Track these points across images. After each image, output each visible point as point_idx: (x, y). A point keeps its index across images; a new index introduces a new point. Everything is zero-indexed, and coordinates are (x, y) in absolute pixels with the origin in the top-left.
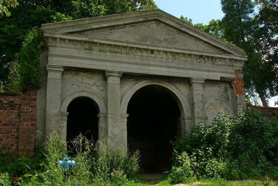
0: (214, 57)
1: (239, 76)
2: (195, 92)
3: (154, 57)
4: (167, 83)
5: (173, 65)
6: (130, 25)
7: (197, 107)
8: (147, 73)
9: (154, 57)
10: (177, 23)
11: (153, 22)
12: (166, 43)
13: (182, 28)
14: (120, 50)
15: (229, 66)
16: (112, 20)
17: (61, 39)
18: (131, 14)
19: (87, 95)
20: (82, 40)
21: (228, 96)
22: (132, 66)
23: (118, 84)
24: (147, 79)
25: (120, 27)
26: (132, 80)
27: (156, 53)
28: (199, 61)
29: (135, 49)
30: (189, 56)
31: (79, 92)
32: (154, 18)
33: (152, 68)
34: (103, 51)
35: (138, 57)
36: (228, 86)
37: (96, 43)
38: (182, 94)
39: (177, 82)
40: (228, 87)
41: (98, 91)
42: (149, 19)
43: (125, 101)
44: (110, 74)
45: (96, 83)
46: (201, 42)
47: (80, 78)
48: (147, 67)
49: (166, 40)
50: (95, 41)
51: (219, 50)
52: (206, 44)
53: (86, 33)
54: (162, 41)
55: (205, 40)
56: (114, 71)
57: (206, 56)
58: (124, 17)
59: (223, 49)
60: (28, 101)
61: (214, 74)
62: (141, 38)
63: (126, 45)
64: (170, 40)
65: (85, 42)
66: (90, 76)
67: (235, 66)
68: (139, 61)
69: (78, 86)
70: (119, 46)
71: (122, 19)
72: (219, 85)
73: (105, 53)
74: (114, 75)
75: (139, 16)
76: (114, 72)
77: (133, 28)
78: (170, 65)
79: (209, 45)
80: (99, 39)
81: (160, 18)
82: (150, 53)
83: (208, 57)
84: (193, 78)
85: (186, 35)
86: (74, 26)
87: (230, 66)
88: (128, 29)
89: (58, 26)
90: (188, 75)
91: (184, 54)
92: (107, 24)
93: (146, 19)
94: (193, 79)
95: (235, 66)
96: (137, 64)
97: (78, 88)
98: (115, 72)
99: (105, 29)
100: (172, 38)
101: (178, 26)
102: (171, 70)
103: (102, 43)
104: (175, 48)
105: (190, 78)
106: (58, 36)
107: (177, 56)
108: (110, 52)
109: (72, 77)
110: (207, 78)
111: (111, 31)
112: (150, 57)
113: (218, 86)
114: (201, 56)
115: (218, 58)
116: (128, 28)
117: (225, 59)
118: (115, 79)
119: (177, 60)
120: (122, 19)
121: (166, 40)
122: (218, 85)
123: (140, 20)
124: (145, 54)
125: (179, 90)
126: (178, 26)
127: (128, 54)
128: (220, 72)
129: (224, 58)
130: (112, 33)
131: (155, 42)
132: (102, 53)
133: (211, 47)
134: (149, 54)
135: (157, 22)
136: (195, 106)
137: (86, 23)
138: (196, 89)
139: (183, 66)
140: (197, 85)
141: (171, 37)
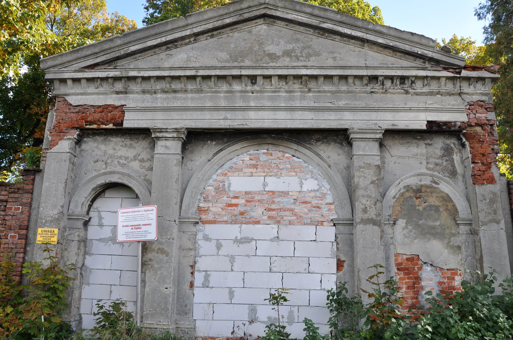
0: (407, 77)
1: (480, 117)
2: (357, 162)
3: (258, 92)
4: (293, 144)
5: (305, 104)
6: (207, 35)
7: (363, 196)
8: (241, 127)
9: (258, 92)
10: (312, 15)
11: (258, 21)
12: (288, 59)
13: (324, 22)
14: (182, 85)
15: (450, 94)
16: (167, 31)
17: (76, 80)
18: (205, 11)
19: (120, 178)
20: (109, 76)
21: (453, 166)
22: (207, 115)
23: (174, 154)
24: (247, 139)
25: (187, 41)
26: (214, 143)
27: (260, 80)
28: (369, 89)
29: (213, 79)
30: (343, 82)
31: (105, 174)
32: (257, 13)
33: (252, 114)
34: (148, 92)
35: (222, 95)
36: (452, 142)
37: (134, 78)
38: (329, 166)
39: (319, 141)
40: (452, 145)
41: (143, 170)
42: (247, 16)
43: (194, 188)
44: (158, 135)
45: (139, 155)
46: (375, 48)
47: (110, 148)
48: (240, 115)
49: (287, 53)
50: (132, 74)
51: (422, 60)
52: (386, 50)
53: (120, 63)
54: (279, 57)
55: (380, 40)
56: (167, 129)
57: (387, 77)
58: (190, 20)
59: (430, 56)
60: (19, 195)
61: (411, 115)
62: (231, 57)
63: (192, 73)
64: (298, 52)
65: (116, 79)
66: (128, 142)
67: (468, 94)
68: (223, 103)
69: (106, 163)
70: (178, 78)
71: (187, 25)
72: (429, 141)
73: (154, 95)
74: (168, 135)
75: (224, 13)
76: (166, 130)
77: (214, 39)
78: (297, 104)
79: (395, 53)
80: (139, 70)
81: (273, 11)
82: (250, 84)
83: (391, 78)
84: (353, 129)
85: (336, 36)
86: (96, 53)
87: (453, 94)
88: (205, 42)
89: (67, 58)
90: (343, 122)
91: (328, 78)
92: (159, 39)
93: (241, 18)
94: (351, 131)
95: (468, 94)
96: (216, 109)
97: (104, 166)
98: (168, 130)
99: (157, 50)
100: (303, 47)
101: (314, 22)
102: (298, 115)
103: (145, 75)
104: (306, 67)
105: (346, 130)
106: (66, 76)
107: (312, 84)
108: (164, 91)
109: (97, 147)
110: (390, 127)
111: (170, 52)
112: (247, 92)
113: (426, 144)
114: (374, 79)
115: (417, 77)
116: (204, 42)
117: (438, 78)
118: (169, 143)
119: (314, 92)
120: (187, 25)
121: (287, 53)
122: (426, 142)
123: (228, 21)
124: (237, 87)
125: (321, 158)
126: (315, 21)
127: (200, 91)
128: (426, 110)
129: (433, 78)
130: (171, 55)
131: (261, 60)
132: (148, 96)
133: (400, 56)
134: (246, 86)
135: (268, 20)
136: (360, 192)
137: (116, 44)
138: (361, 153)
139: (329, 105)
140: (362, 144)
141: (300, 45)
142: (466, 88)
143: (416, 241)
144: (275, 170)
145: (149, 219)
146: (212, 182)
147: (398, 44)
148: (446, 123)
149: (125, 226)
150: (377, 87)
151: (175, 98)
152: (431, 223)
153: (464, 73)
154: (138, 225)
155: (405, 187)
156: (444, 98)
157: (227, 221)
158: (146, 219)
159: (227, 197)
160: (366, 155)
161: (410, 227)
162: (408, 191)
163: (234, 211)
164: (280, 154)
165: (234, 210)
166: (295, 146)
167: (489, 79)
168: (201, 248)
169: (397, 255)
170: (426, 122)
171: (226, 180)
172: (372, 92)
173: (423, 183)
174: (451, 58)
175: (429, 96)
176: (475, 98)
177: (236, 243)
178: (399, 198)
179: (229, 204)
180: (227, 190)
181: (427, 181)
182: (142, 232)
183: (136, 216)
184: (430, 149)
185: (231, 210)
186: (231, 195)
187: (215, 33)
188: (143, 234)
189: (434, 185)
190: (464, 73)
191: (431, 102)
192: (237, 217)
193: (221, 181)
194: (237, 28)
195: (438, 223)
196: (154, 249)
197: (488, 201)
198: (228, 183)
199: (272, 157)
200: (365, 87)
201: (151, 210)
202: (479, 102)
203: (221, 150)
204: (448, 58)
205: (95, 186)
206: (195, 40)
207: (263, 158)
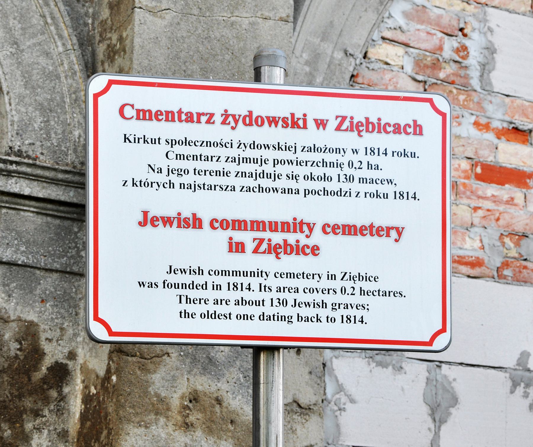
145: (383, 189)
146: (401, 21)
149: (167, 221)
154: (286, 227)
157: (477, 263)
158: (355, 187)
159: (476, 124)
163: (512, 210)
165: (511, 201)
168: (349, 406)
171: (476, 24)
177: (520, 390)
179: (486, 167)
180: (475, 83)
182: (325, 284)
183: (271, 155)
185: (495, 199)
188: (329, 299)
192: (524, 242)
193: (445, 21)
196: (161, 400)
198: (483, 42)
201: (398, 129)
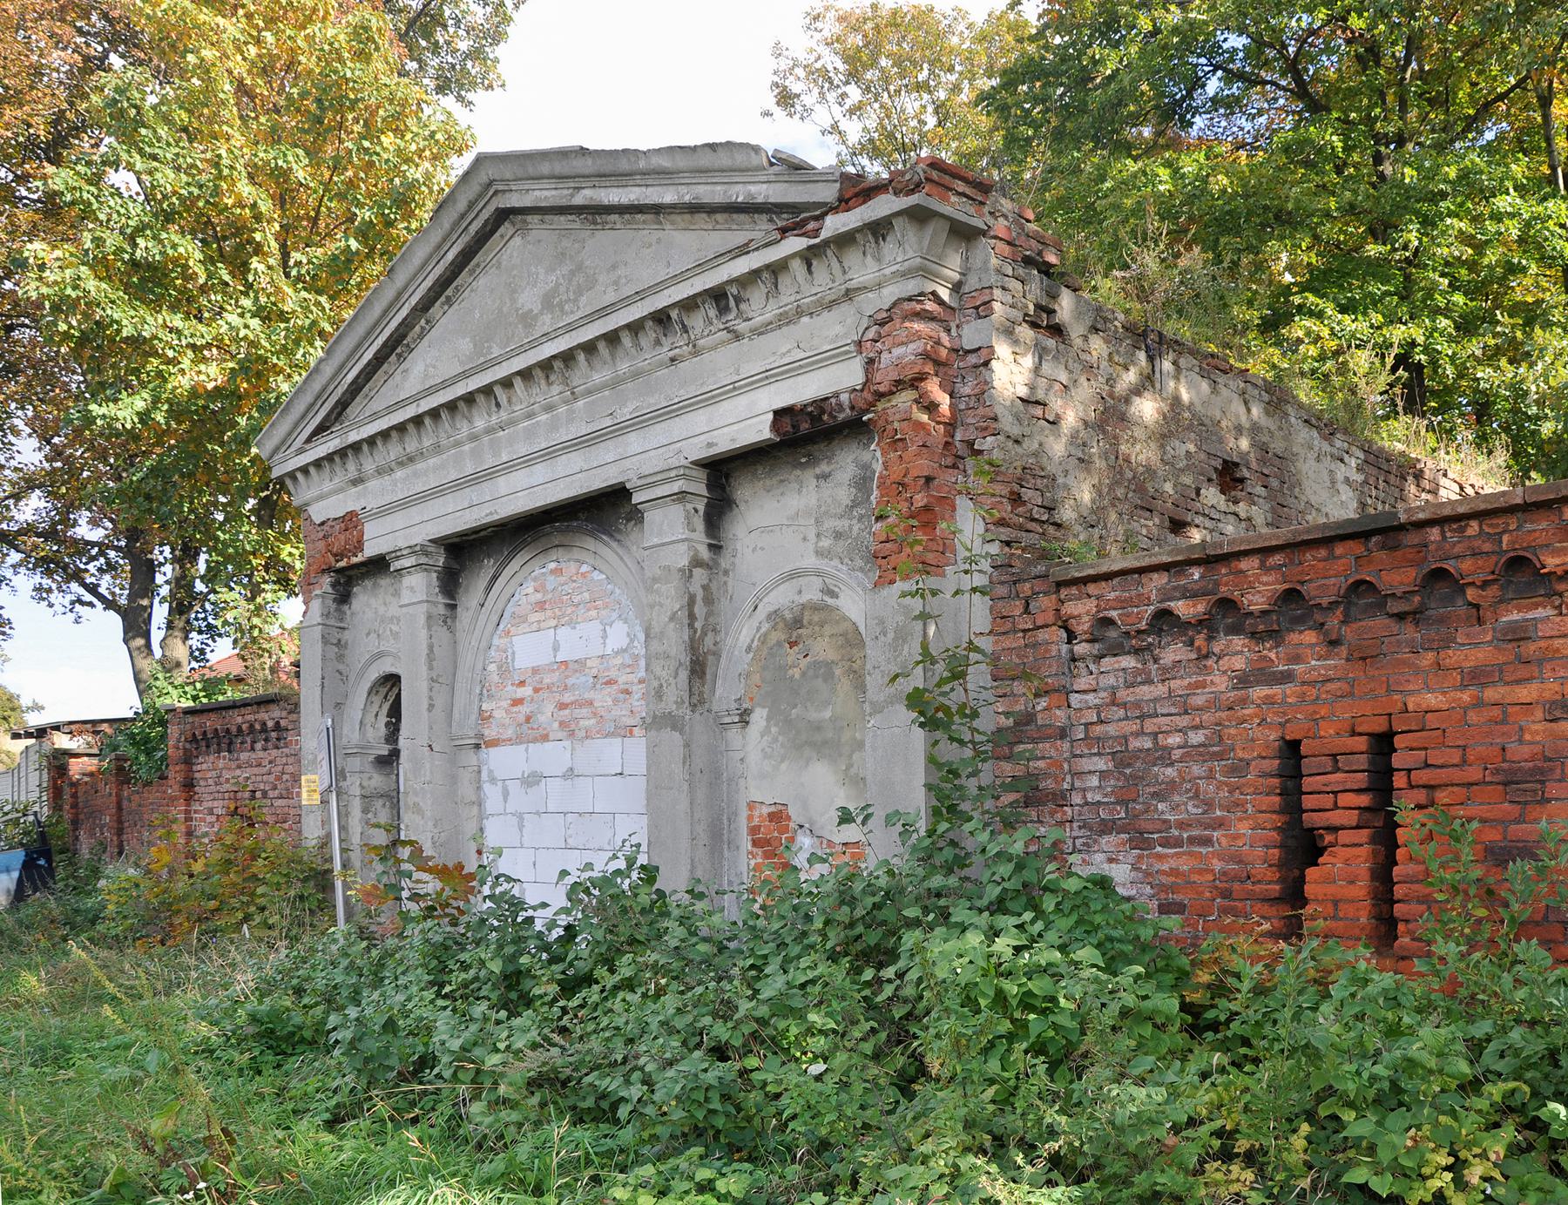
5: (564, 434)
6: (438, 304)
28: (665, 352)
55: (669, 197)
63: (410, 412)
113: (818, 477)
114: (661, 318)
122: (818, 471)
138: (656, 541)
142: (862, 268)
143: (784, 766)
144: (569, 610)
147: (701, 189)
148: (821, 403)
150: (676, 343)
151: (416, 474)
152: (814, 715)
153: (834, 224)
155: (769, 617)
156: (818, 321)
160: (663, 545)
161: (773, 729)
162: (774, 628)
164: (573, 566)
166: (590, 543)
167: (900, 219)
169: (751, 805)
170: (770, 416)
172: (673, 360)
173: (804, 598)
174: (809, 186)
175: (785, 329)
176: (890, 293)
178: (758, 649)
181: (812, 594)
184: (827, 489)
186: (517, 680)
187: (449, 292)
189: (830, 601)
190: (834, 224)
191: (780, 347)
194: (478, 265)
195: (827, 714)
197: (891, 635)
199: (562, 579)
200: (659, 350)
202: (907, 306)
203: (495, 578)
204: (801, 187)
205: (369, 685)
206: (428, 322)
207: (551, 582)
